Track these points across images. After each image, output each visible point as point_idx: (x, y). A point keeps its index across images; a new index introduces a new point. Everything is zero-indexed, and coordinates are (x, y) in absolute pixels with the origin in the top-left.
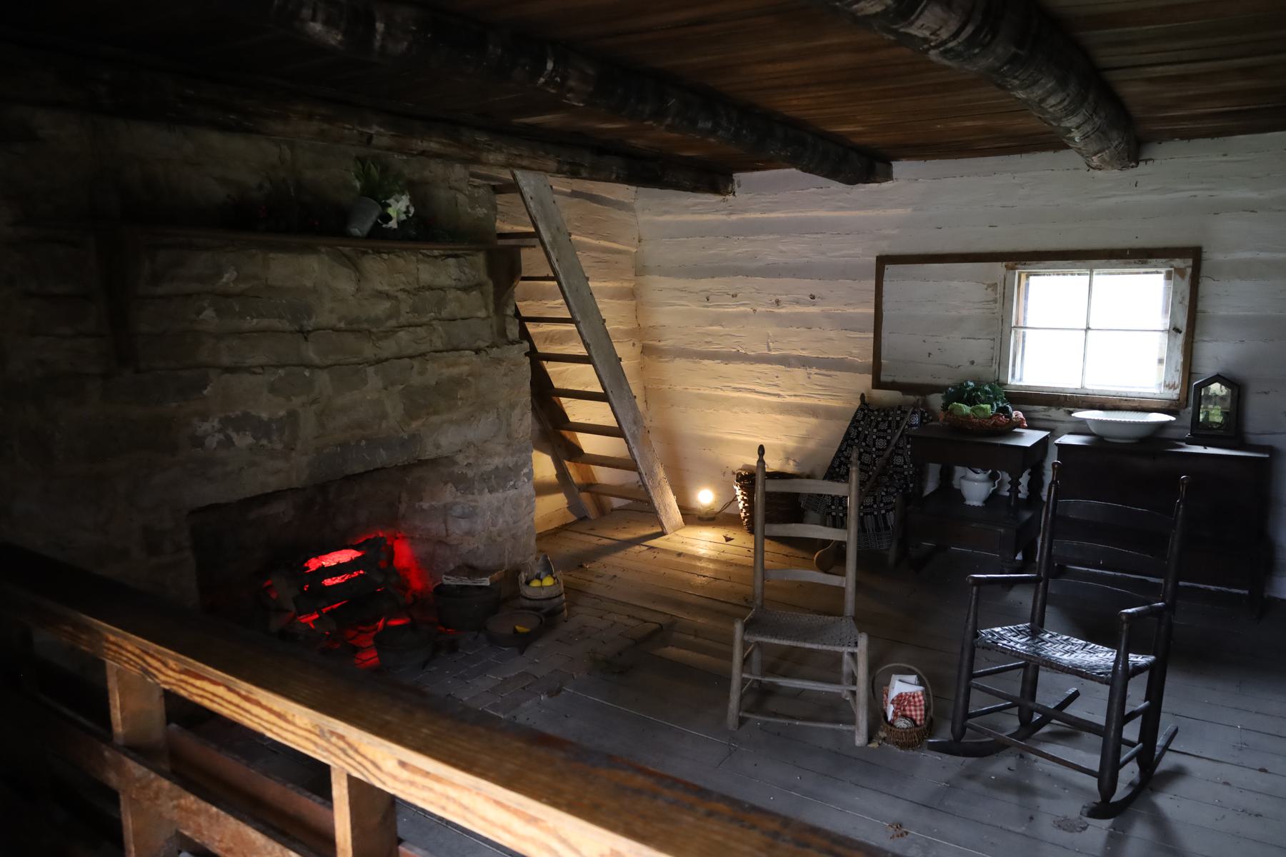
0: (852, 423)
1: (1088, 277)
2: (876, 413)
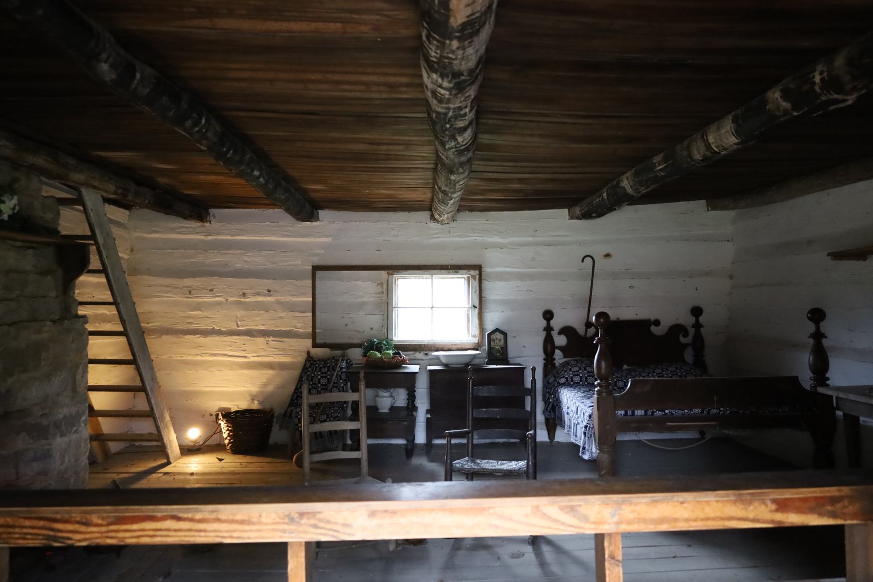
0: (303, 369)
1: (431, 280)
2: (318, 362)
